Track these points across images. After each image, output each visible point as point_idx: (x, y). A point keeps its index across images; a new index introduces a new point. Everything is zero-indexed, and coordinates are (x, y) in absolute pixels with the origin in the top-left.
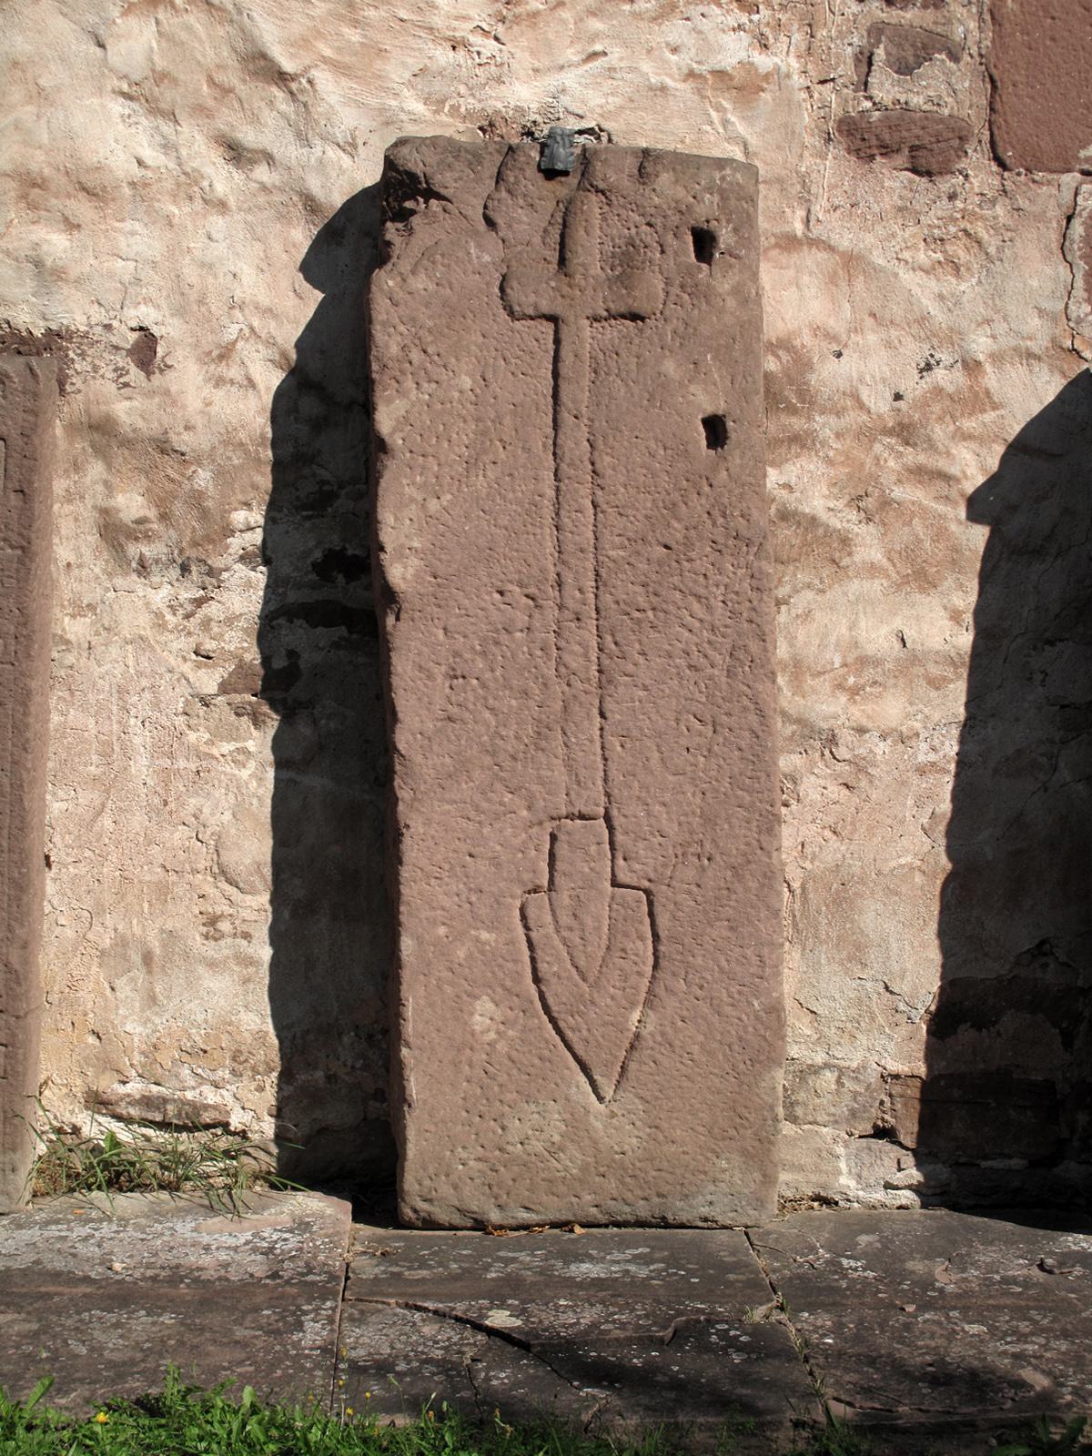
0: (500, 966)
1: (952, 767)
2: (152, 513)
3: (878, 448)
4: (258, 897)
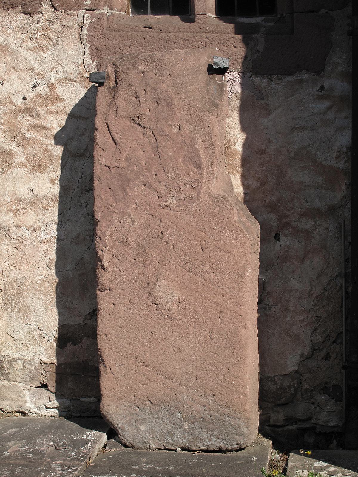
3: (19, 118)
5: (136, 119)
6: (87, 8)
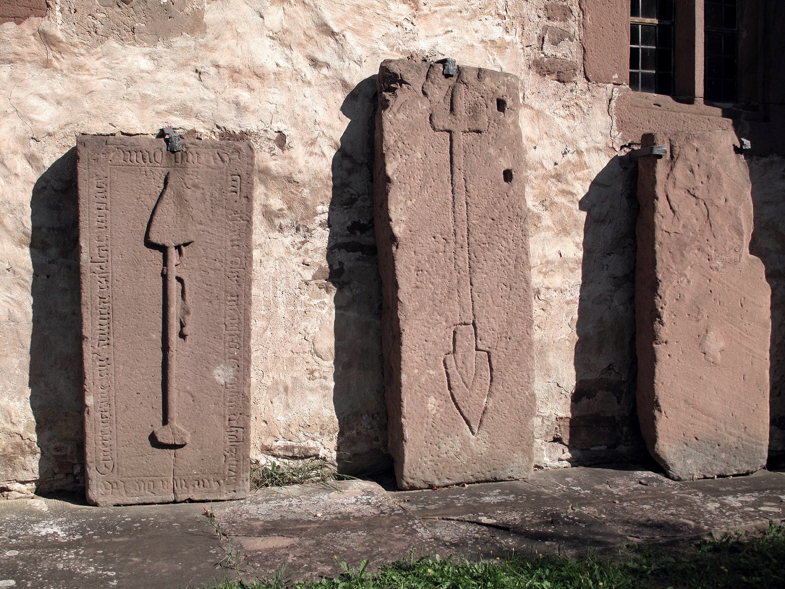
0: (437, 384)
1: (578, 301)
2: (285, 207)
3: (549, 182)
4: (329, 362)
5: (691, 191)
6: (615, 82)
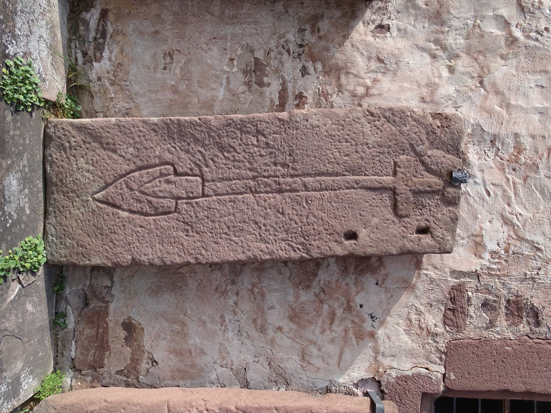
6: (447, 375)
